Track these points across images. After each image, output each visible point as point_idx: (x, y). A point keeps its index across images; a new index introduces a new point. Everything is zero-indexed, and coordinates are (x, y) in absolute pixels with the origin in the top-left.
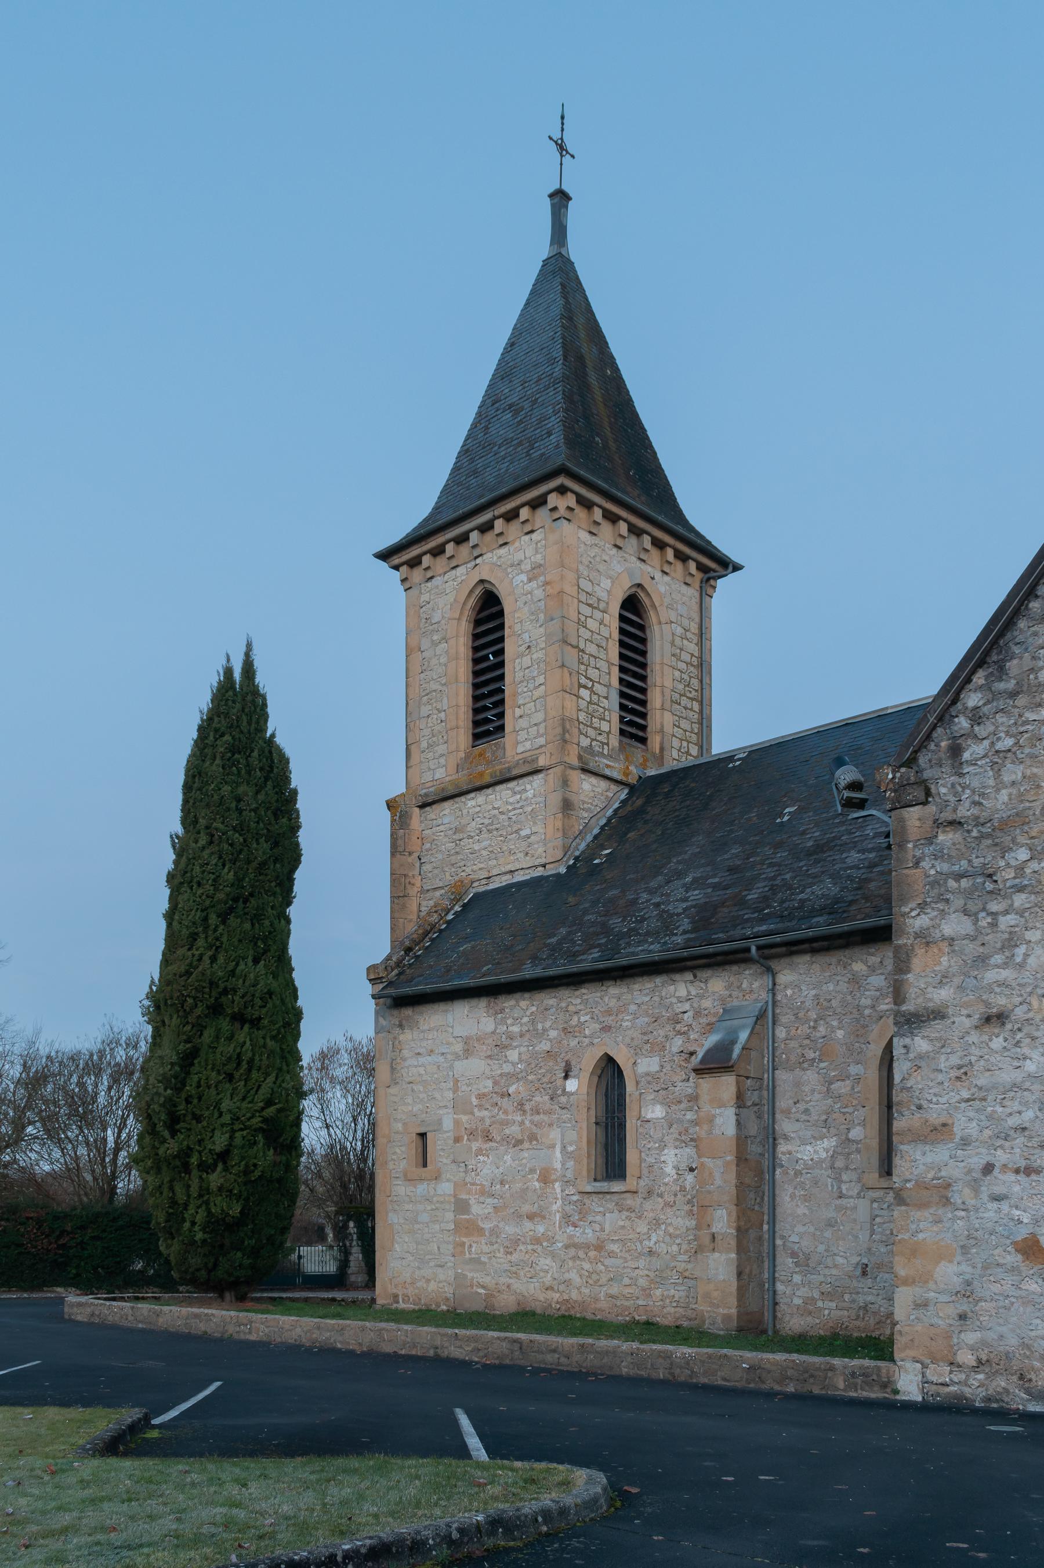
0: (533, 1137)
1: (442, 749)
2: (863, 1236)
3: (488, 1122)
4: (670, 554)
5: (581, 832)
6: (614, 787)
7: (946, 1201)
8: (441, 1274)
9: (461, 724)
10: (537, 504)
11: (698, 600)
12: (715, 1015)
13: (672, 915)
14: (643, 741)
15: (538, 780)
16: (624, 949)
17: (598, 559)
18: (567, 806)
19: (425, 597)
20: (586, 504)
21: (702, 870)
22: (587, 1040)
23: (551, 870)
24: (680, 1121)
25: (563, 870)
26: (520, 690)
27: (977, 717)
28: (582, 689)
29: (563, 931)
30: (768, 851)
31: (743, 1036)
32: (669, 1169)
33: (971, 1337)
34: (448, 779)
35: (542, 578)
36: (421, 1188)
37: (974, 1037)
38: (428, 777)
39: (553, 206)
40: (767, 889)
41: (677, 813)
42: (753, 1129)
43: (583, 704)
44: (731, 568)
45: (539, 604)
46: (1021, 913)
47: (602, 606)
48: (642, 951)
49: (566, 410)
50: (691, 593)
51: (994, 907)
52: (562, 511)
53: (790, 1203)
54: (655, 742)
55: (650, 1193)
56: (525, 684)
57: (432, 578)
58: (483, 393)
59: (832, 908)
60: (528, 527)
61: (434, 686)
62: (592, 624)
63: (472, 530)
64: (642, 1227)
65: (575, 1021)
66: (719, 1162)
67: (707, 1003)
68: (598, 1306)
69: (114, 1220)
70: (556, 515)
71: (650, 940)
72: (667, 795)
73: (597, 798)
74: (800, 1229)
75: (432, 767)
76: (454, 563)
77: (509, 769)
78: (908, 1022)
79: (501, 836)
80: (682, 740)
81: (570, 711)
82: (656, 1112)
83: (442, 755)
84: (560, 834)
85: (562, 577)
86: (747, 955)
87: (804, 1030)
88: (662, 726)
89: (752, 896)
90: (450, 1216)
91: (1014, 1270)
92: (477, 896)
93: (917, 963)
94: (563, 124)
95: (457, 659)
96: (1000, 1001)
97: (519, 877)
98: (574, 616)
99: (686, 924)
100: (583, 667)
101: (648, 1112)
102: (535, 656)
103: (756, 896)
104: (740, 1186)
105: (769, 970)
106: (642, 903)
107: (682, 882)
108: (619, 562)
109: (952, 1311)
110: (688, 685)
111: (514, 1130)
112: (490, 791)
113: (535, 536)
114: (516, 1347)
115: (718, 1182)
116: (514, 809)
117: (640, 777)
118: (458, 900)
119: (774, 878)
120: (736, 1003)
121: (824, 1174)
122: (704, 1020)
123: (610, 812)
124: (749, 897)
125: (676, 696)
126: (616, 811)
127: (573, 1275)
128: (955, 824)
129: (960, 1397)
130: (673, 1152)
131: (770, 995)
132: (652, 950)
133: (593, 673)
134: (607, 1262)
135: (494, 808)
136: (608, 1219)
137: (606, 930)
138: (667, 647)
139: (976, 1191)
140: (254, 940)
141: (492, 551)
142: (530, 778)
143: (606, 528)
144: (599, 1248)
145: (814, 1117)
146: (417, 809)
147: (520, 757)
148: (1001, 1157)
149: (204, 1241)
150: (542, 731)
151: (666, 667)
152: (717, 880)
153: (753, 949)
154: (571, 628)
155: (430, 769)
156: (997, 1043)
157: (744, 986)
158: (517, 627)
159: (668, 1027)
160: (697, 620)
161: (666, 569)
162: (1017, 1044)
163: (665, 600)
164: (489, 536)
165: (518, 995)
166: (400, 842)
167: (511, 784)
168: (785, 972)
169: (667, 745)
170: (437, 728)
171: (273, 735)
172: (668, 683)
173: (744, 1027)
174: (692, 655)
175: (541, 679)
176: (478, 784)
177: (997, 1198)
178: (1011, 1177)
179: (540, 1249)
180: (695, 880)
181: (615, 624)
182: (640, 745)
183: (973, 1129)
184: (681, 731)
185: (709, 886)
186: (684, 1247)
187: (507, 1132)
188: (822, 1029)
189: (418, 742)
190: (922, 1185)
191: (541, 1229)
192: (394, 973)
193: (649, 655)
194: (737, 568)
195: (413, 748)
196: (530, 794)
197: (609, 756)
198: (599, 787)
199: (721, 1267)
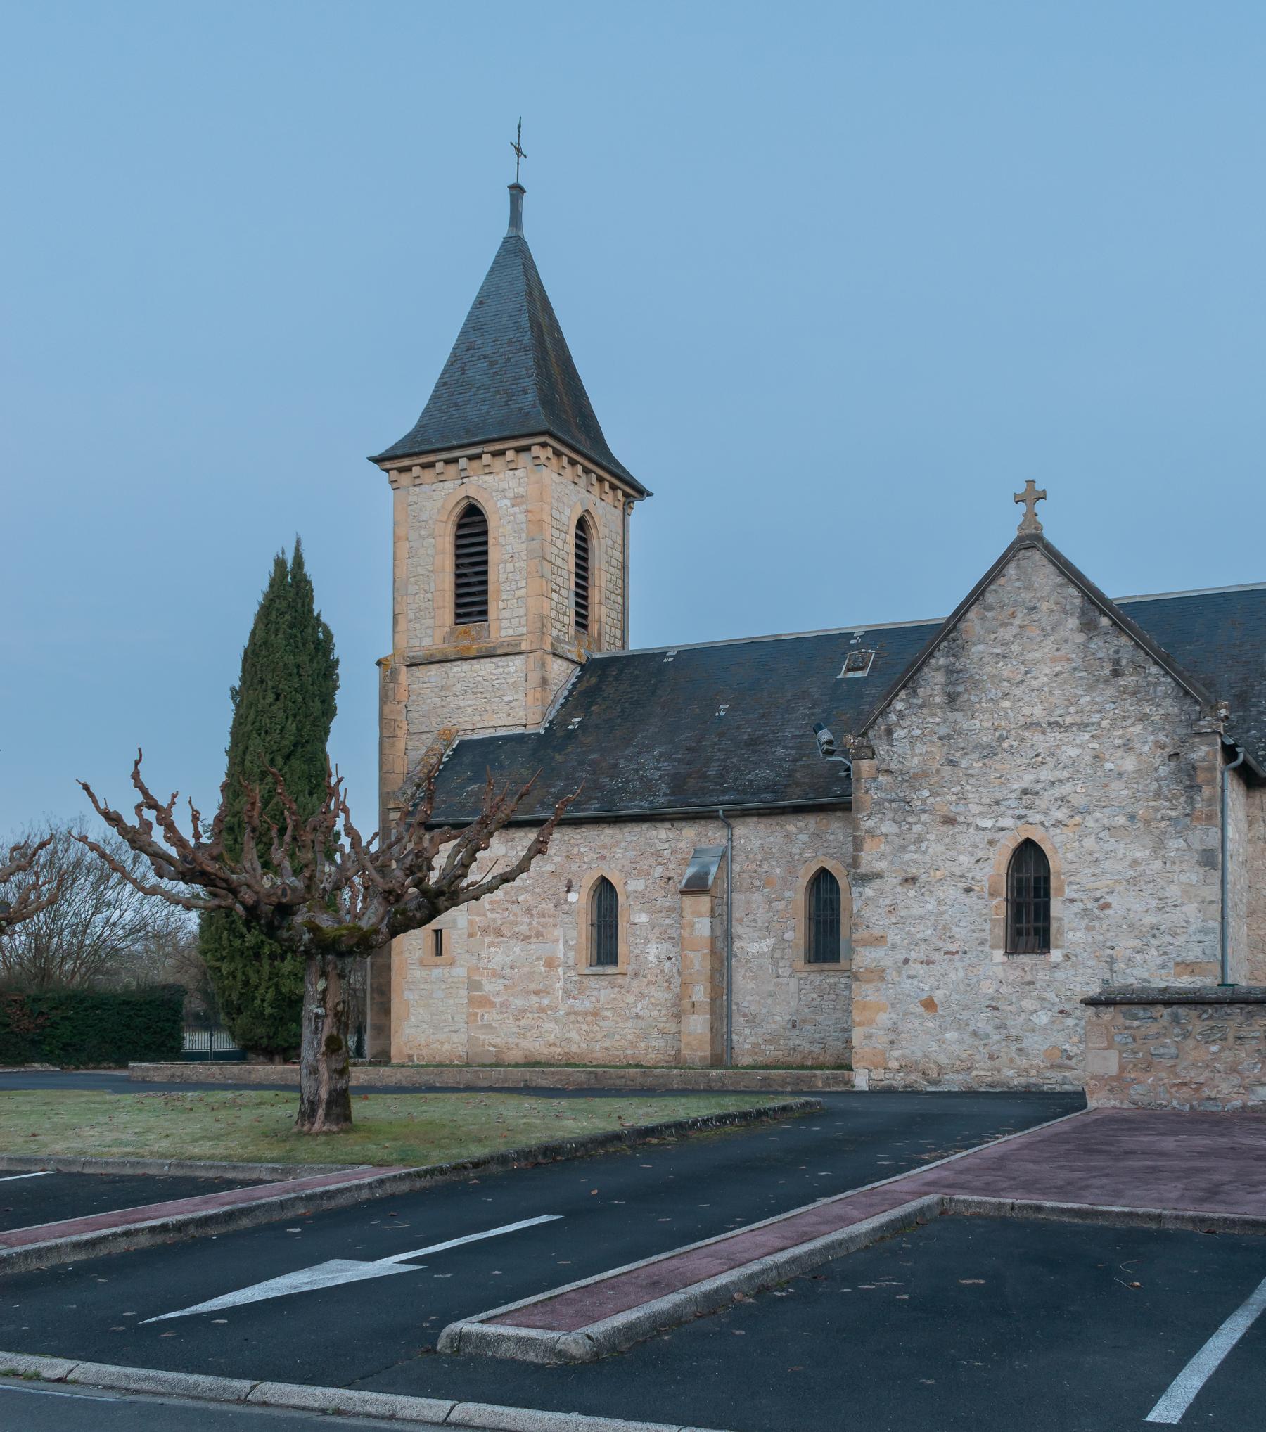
0: (539, 934)
2: (793, 1003)
3: (499, 922)
6: (572, 666)
7: (883, 979)
8: (455, 1037)
9: (447, 605)
12: (688, 853)
15: (519, 660)
18: (544, 682)
19: (414, 499)
22: (586, 866)
23: (531, 730)
24: (661, 925)
27: (901, 716)
31: (714, 869)
32: (652, 958)
33: (896, 1053)
36: (437, 972)
37: (899, 889)
38: (415, 642)
39: (512, 195)
42: (719, 932)
46: (925, 824)
51: (910, 820)
52: (543, 460)
53: (743, 982)
55: (636, 975)
59: (772, 788)
60: (512, 466)
61: (420, 570)
62: (560, 544)
64: (630, 999)
65: (576, 850)
66: (698, 954)
67: (682, 845)
68: (594, 1056)
69: (81, 1002)
70: (537, 462)
72: (616, 678)
73: (561, 673)
74: (749, 998)
78: (861, 879)
81: (547, 612)
82: (643, 918)
87: (753, 866)
90: (464, 993)
91: (920, 1016)
92: (462, 743)
93: (866, 846)
96: (913, 871)
97: (501, 732)
99: (664, 789)
101: (635, 919)
104: (713, 970)
105: (729, 826)
109: (886, 1039)
111: (523, 929)
112: (475, 662)
114: (593, 1076)
115: (697, 967)
119: (724, 760)
120: (704, 846)
121: (767, 962)
122: (680, 856)
123: (569, 686)
127: (574, 1035)
128: (889, 772)
129: (892, 1086)
130: (655, 946)
132: (644, 807)
134: (602, 1024)
136: (602, 992)
139: (900, 973)
140: (309, 778)
143: (569, 471)
144: (595, 1014)
145: (759, 924)
148: (913, 955)
149: (271, 1015)
150: (524, 623)
154: (547, 547)
156: (912, 893)
158: (501, 540)
159: (652, 859)
162: (923, 894)
165: (527, 829)
170: (424, 605)
171: (319, 615)
172: (603, 585)
173: (712, 863)
176: (466, 655)
177: (911, 977)
178: (919, 965)
179: (544, 1016)
180: (662, 754)
183: (898, 940)
185: (675, 760)
186: (664, 1012)
187: (517, 930)
188: (765, 867)
190: (868, 970)
191: (545, 1002)
194: (650, 494)
197: (569, 643)
199: (698, 1025)
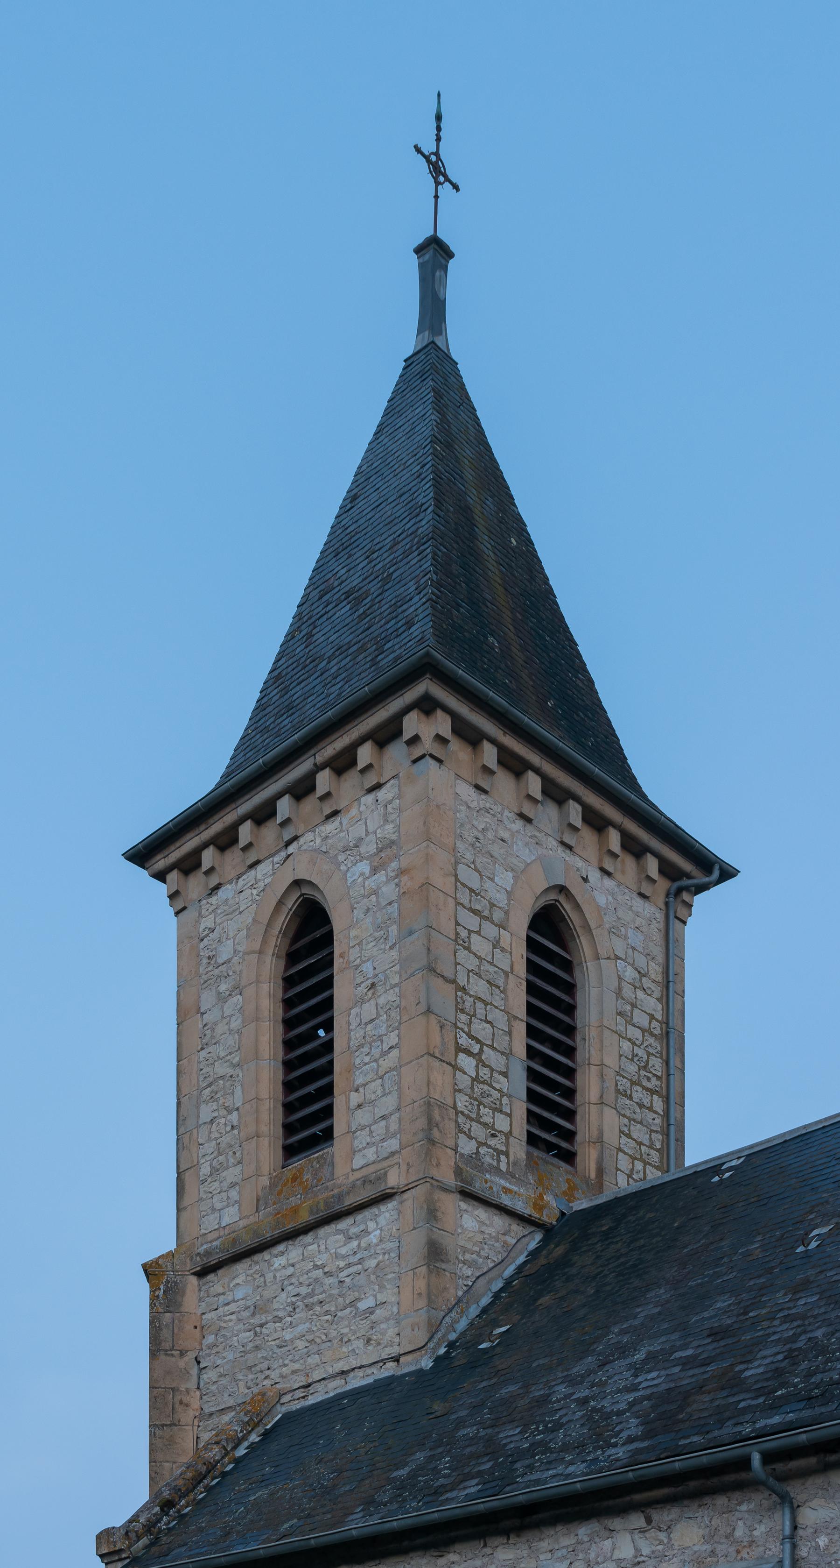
1: (232, 1174)
4: (614, 839)
5: (459, 1301)
6: (517, 1229)
9: (264, 1129)
10: (387, 735)
11: (662, 925)
13: (608, 1416)
14: (569, 1157)
15: (387, 1212)
16: (522, 1476)
17: (490, 835)
18: (435, 1253)
19: (207, 922)
20: (471, 737)
21: (663, 1339)
23: (408, 1365)
25: (427, 1363)
26: (357, 1061)
28: (462, 1056)
29: (421, 1456)
30: (781, 1297)
34: (242, 1223)
35: (394, 865)
38: (210, 1223)
39: (422, 266)
40: (780, 1357)
41: (622, 1260)
43: (464, 1081)
44: (716, 874)
45: (390, 909)
47: (497, 916)
48: (554, 1476)
49: (438, 585)
50: (650, 913)
52: (428, 744)
54: (588, 1159)
56: (366, 1049)
57: (217, 887)
58: (306, 582)
60: (371, 779)
61: (221, 1069)
63: (280, 795)
70: (417, 752)
71: (569, 1458)
73: (487, 1244)
75: (218, 1206)
76: (252, 857)
77: (340, 1197)
79: (327, 1313)
80: (633, 1158)
83: (233, 1185)
84: (422, 1303)
85: (428, 859)
86: (743, 1476)
88: (601, 1133)
89: (754, 1371)
92: (288, 1418)
94: (439, 129)
95: (257, 1019)
97: (356, 1381)
98: (448, 928)
99: (633, 1426)
100: (463, 1017)
102: (382, 1001)
103: (761, 1370)
105: (785, 1499)
106: (558, 1401)
107: (628, 1361)
108: (526, 844)
110: (645, 1068)
112: (309, 1238)
113: (382, 794)
116: (349, 1265)
117: (563, 1214)
118: (257, 1425)
119: (794, 1339)
123: (510, 1271)
124: (748, 1373)
125: (624, 1084)
126: (520, 1269)
131: (788, 1547)
133: (481, 1030)
135: (316, 1267)
137: (492, 1448)
138: (610, 998)
141: (312, 830)
142: (374, 1210)
143: (504, 781)
146: (194, 1280)
147: (358, 1175)
150: (394, 1127)
151: (607, 1033)
152: (689, 1352)
153: (756, 1459)
155: (213, 1210)
157: (739, 1533)
158: (354, 954)
160: (660, 958)
161: (609, 865)
163: (606, 919)
164: (310, 803)
166: (165, 1334)
167: (344, 1224)
168: (815, 1503)
169: (608, 1164)
170: (226, 1139)
172: (611, 1060)
174: (652, 1017)
175: (393, 1039)
176: (290, 1226)
180: (651, 1357)
181: (521, 950)
182: (562, 1164)
184: (633, 1144)
189: (196, 1166)
192: (141, 1544)
193: (578, 1013)
194: (727, 873)
195: (187, 1176)
196: (374, 1238)
197: (510, 1175)
198: (491, 1225)
